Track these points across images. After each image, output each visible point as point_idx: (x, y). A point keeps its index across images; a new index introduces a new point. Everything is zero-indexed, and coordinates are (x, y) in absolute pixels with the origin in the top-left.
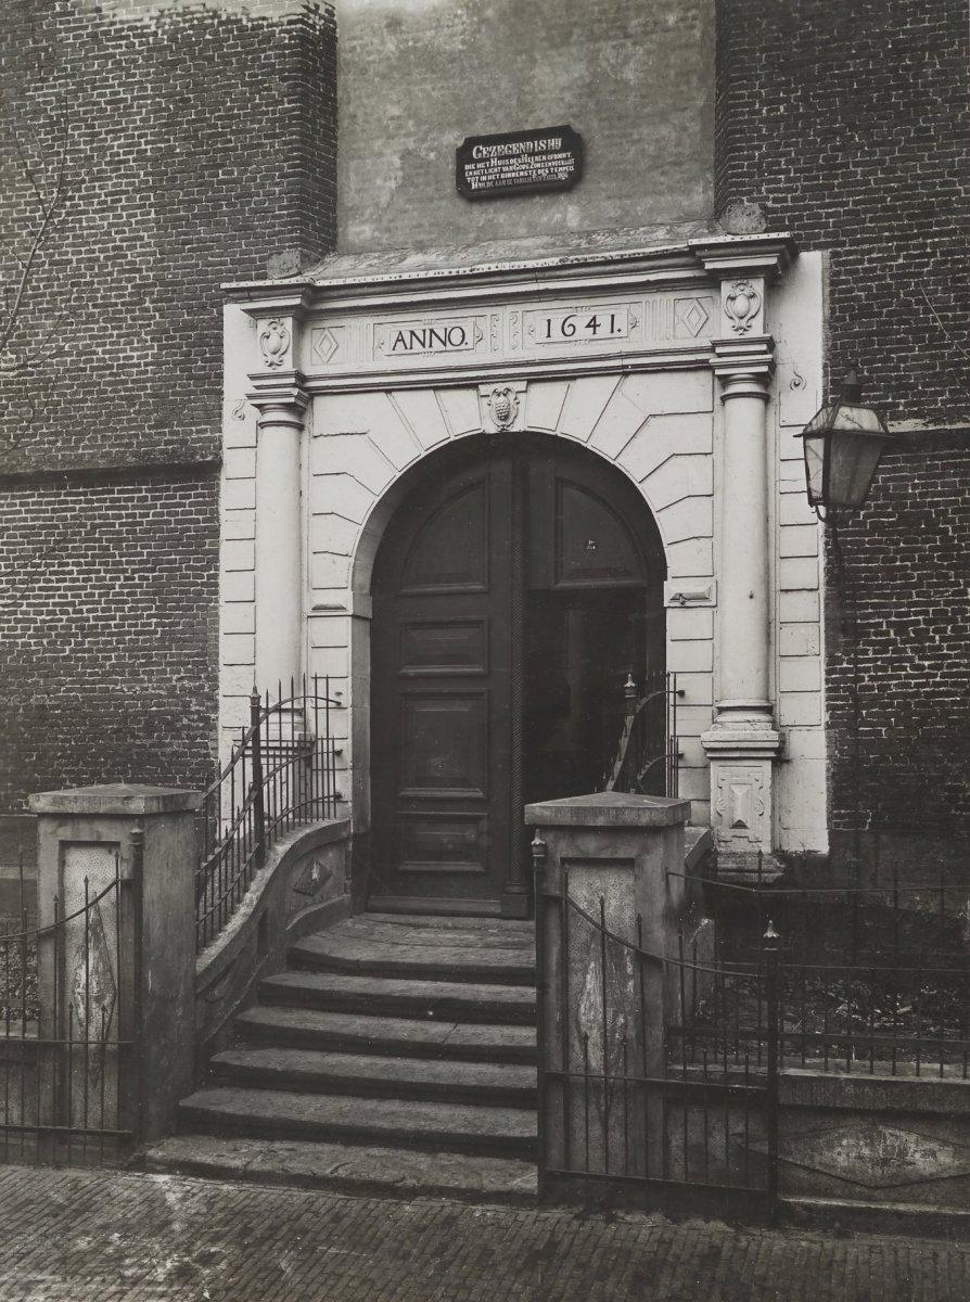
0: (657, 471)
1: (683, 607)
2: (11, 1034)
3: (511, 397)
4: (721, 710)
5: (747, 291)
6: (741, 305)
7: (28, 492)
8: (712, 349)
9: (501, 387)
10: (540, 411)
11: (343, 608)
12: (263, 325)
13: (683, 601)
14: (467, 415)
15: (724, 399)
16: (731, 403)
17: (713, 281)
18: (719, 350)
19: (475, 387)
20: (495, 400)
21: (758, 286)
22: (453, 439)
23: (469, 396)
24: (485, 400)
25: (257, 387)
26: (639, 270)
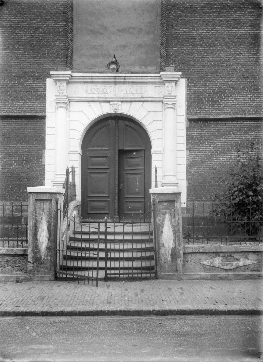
0: (19, 121)
1: (156, 153)
2: (194, 236)
3: (118, 105)
4: (164, 176)
5: (171, 85)
6: (170, 88)
7: (256, 122)
8: (163, 98)
9: (116, 103)
10: (125, 109)
11: (161, 152)
12: (58, 84)
13: (156, 153)
14: (106, 109)
15: (57, 108)
16: (59, 109)
17: (163, 83)
18: (165, 98)
19: (109, 102)
20: (114, 105)
21: (174, 84)
22: (104, 114)
23: (107, 104)
24: (111, 106)
25: (56, 98)
26: (88, 79)
